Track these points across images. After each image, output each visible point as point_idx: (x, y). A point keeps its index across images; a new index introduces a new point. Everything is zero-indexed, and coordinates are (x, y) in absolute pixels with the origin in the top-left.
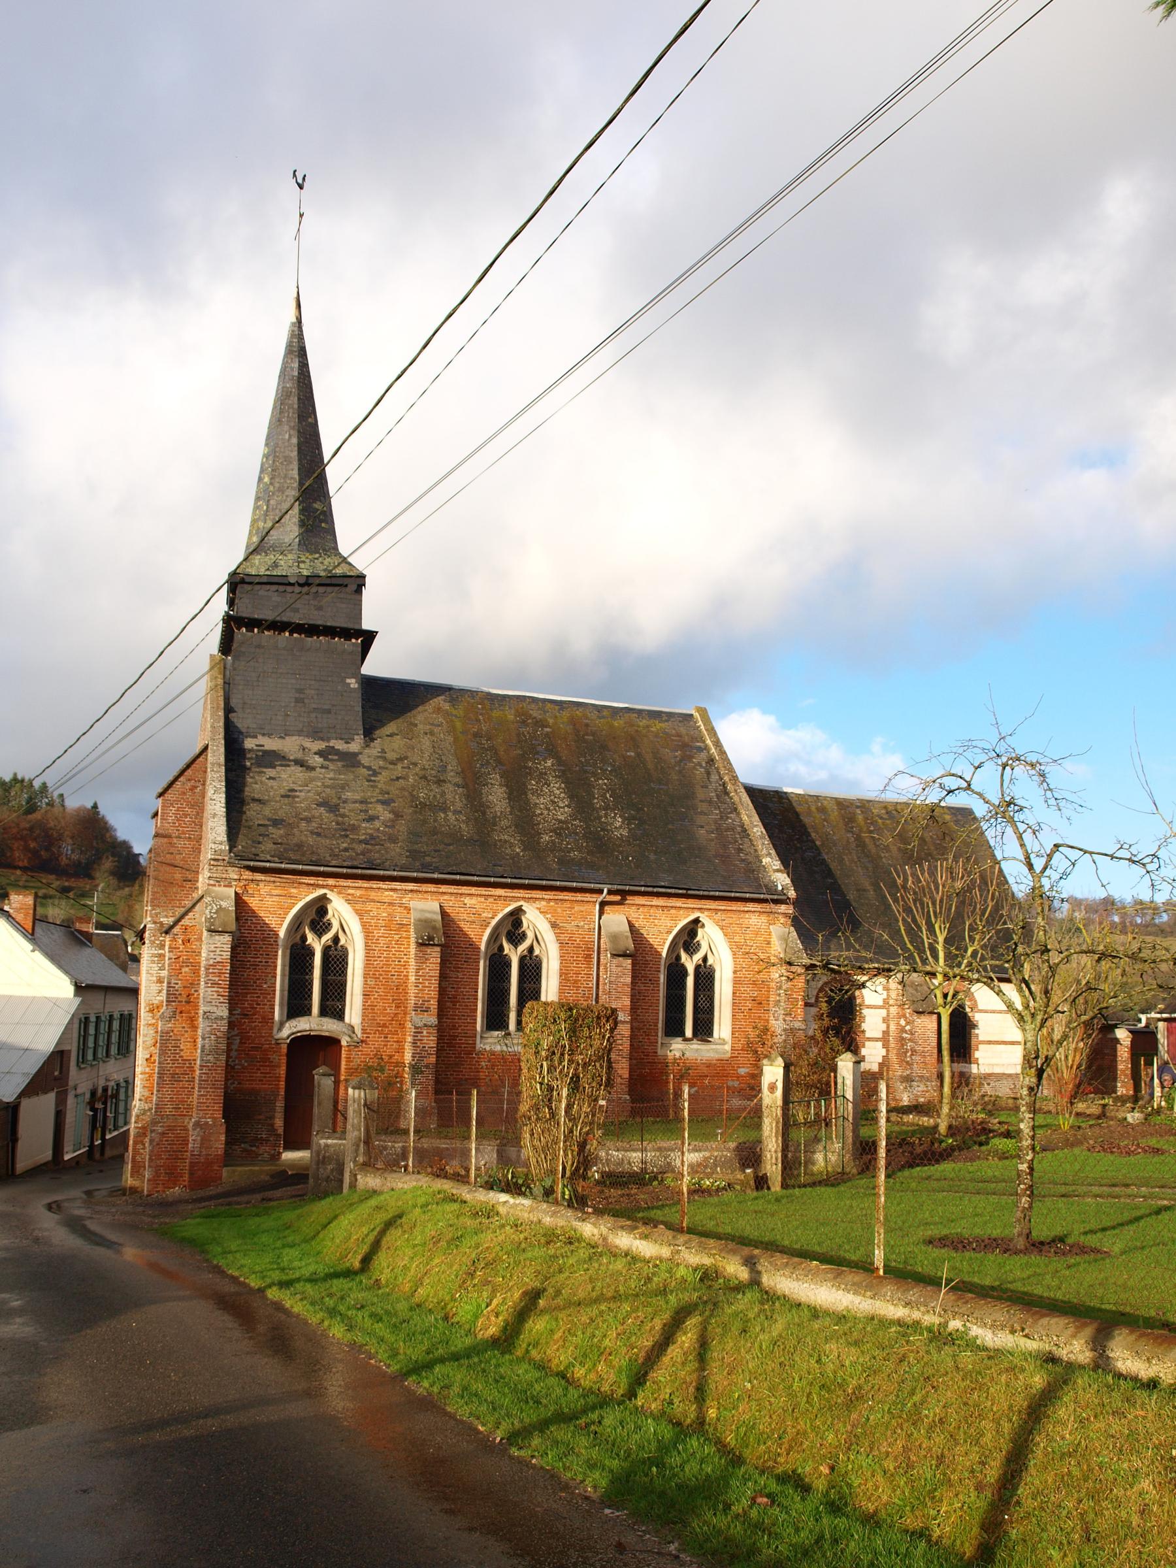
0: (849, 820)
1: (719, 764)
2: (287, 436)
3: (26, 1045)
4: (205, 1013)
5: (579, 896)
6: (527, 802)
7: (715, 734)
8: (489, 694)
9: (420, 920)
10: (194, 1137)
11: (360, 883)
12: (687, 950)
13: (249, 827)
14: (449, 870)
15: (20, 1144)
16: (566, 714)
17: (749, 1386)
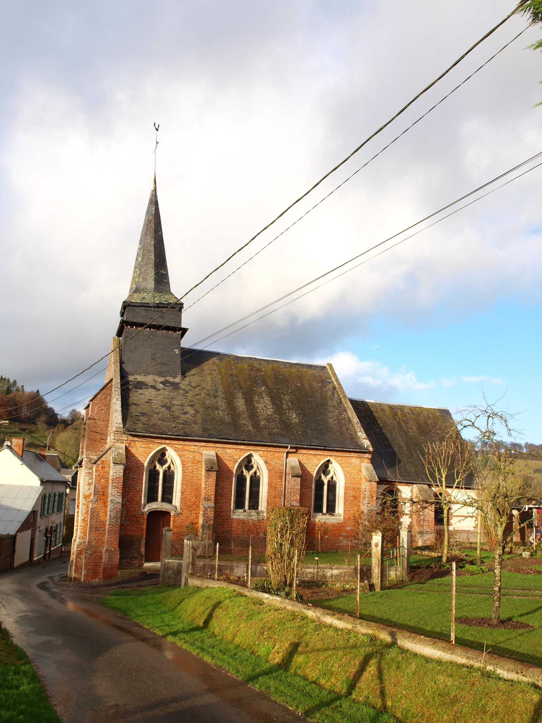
0: (395, 415)
1: (338, 389)
2: (149, 241)
3: (19, 508)
4: (111, 500)
5: (277, 450)
6: (254, 406)
7: (336, 376)
8: (236, 356)
9: (207, 460)
10: (105, 557)
11: (181, 442)
12: (324, 474)
13: (132, 416)
14: (220, 437)
15: (16, 554)
16: (270, 366)
17: (404, 692)
